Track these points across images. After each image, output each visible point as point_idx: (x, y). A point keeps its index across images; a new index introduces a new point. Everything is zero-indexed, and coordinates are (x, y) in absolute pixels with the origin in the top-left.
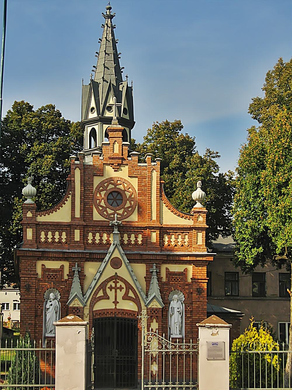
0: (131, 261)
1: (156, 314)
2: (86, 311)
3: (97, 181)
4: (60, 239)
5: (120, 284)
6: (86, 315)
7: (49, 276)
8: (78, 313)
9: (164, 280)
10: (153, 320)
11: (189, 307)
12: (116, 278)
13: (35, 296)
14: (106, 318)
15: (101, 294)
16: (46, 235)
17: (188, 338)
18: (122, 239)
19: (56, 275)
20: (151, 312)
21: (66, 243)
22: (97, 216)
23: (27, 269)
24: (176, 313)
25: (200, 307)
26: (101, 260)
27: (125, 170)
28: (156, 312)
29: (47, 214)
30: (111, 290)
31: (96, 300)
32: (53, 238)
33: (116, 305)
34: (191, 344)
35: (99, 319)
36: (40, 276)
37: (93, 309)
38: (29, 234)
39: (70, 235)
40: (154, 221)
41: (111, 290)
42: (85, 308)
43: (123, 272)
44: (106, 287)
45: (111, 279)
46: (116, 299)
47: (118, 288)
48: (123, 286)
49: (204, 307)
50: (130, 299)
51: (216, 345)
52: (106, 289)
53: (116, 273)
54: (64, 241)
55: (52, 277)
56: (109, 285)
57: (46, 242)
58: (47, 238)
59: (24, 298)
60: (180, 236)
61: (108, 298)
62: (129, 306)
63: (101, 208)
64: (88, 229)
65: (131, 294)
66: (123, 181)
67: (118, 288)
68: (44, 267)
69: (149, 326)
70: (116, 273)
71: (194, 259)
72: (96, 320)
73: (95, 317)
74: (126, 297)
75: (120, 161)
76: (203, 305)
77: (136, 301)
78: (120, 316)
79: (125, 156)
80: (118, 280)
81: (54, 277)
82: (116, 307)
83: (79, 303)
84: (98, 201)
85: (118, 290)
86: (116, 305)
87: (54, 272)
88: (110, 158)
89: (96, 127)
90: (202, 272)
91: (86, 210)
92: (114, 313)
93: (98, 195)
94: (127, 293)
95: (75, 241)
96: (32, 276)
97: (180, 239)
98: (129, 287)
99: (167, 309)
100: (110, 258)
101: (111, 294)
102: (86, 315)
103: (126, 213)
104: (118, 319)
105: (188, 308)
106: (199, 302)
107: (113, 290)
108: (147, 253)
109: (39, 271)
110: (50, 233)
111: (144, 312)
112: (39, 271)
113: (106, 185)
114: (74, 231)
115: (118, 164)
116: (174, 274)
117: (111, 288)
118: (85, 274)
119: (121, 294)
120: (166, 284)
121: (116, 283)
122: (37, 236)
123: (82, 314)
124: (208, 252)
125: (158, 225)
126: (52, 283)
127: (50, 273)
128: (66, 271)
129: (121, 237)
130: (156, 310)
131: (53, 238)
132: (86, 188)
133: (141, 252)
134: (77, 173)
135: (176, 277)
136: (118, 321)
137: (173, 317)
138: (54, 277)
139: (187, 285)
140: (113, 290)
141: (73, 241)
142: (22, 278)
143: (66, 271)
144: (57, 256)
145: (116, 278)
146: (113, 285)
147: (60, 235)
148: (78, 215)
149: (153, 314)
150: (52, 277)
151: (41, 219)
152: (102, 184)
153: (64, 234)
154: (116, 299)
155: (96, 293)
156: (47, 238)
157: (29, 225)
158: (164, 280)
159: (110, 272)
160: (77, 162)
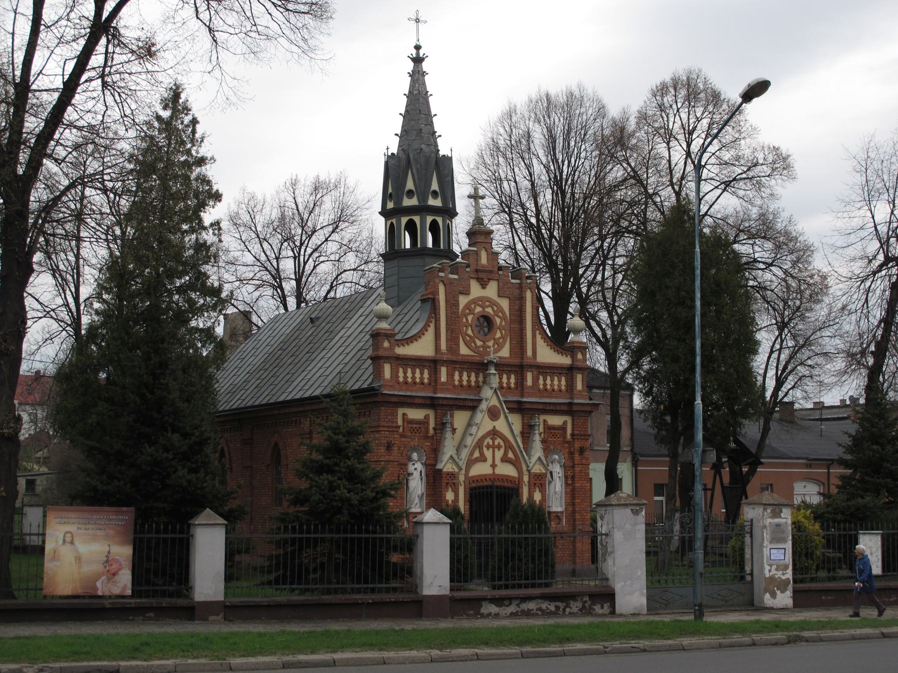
2: (462, 478)
3: (463, 301)
4: (422, 378)
5: (498, 441)
12: (494, 433)
21: (430, 384)
22: (464, 350)
31: (471, 462)
32: (413, 378)
33: (494, 470)
35: (475, 488)
39: (435, 374)
43: (501, 425)
45: (488, 434)
46: (494, 461)
48: (502, 444)
53: (494, 427)
54: (426, 381)
55: (416, 430)
56: (485, 443)
58: (405, 377)
61: (485, 460)
62: (508, 470)
70: (494, 427)
72: (471, 489)
74: (505, 459)
78: (498, 483)
82: (494, 473)
85: (496, 450)
86: (494, 470)
89: (417, 219)
91: (453, 341)
94: (506, 453)
101: (488, 454)
107: (491, 450)
110: (409, 371)
111: (526, 479)
116: (412, 422)
117: (488, 447)
119: (499, 454)
121: (493, 439)
126: (416, 439)
128: (432, 424)
131: (413, 378)
137: (553, 485)
140: (491, 450)
143: (432, 424)
145: (494, 433)
147: (422, 374)
148: (443, 346)
150: (416, 430)
152: (468, 306)
153: (426, 371)
154: (494, 461)
155: (472, 453)
156: (405, 377)
159: (487, 425)
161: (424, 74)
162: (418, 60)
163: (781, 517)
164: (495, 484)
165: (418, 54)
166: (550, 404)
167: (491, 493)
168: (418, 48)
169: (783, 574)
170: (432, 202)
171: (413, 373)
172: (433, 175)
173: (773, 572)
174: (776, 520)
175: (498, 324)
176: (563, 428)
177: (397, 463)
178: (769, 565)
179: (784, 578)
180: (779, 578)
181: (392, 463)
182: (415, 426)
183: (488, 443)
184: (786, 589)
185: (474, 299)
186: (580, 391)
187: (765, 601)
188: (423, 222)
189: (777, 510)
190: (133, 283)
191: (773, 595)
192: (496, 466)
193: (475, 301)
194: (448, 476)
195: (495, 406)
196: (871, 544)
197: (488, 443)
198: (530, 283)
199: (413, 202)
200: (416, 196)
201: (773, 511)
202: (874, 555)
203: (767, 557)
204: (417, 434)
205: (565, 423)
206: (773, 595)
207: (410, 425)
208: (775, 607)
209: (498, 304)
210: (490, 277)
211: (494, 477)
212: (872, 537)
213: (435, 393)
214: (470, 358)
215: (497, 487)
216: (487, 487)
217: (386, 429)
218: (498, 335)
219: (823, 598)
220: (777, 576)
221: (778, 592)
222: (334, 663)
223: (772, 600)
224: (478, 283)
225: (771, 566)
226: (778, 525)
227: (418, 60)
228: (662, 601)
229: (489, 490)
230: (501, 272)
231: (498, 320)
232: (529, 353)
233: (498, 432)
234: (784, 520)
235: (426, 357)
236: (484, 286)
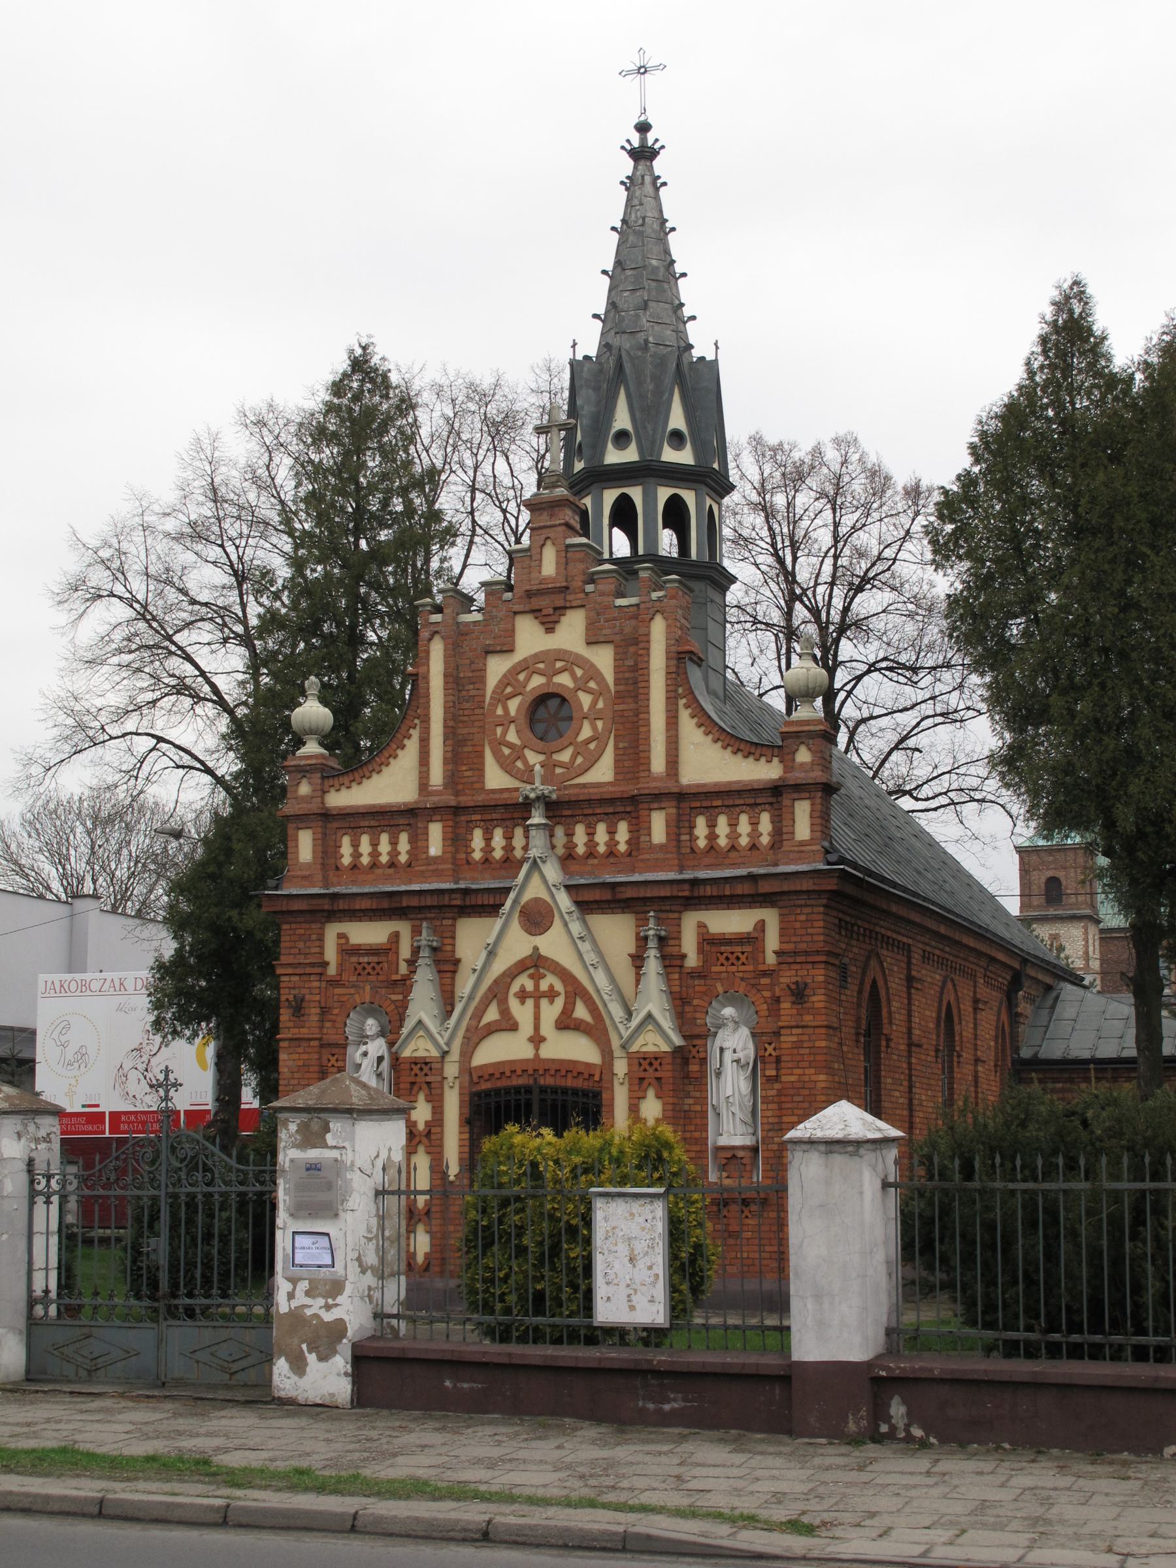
0: (585, 907)
1: (656, 1070)
2: (451, 1070)
4: (394, 853)
6: (451, 1079)
7: (360, 967)
8: (426, 1075)
9: (692, 960)
10: (645, 1091)
11: (770, 1044)
12: (536, 964)
13: (316, 1031)
14: (507, 1091)
15: (492, 1014)
16: (356, 845)
17: (770, 1147)
18: (591, 840)
19: (378, 963)
20: (640, 1064)
22: (495, 778)
23: (297, 951)
24: (729, 1069)
25: (805, 1045)
26: (493, 910)
29: (354, 784)
30: (523, 1003)
31: (477, 1035)
32: (375, 854)
33: (537, 1049)
34: (251, 1168)
35: (487, 1093)
36: (332, 970)
37: (470, 1062)
38: (305, 846)
41: (523, 1003)
42: (448, 1059)
44: (507, 992)
45: (521, 967)
46: (537, 1027)
47: (544, 995)
48: (559, 987)
49: (818, 1044)
50: (577, 1026)
51: (317, 1172)
52: (506, 998)
53: (536, 949)
55: (369, 969)
57: (712, 848)
58: (357, 855)
59: (290, 1036)
61: (513, 1027)
63: (507, 751)
64: (468, 818)
65: (581, 1012)
67: (544, 995)
68: (343, 941)
69: (634, 1109)
72: (478, 1094)
74: (566, 1023)
76: (814, 1037)
77: (596, 1031)
78: (549, 1081)
80: (542, 971)
81: (374, 968)
82: (537, 1055)
83: (430, 1046)
84: (499, 730)
85: (544, 1002)
86: (537, 1049)
87: (372, 954)
89: (636, 494)
90: (810, 931)
92: (531, 1072)
93: (500, 711)
94: (567, 1011)
95: (428, 858)
96: (308, 970)
98: (575, 990)
99: (702, 1055)
100: (515, 901)
101: (522, 1013)
102: (451, 1079)
103: (579, 760)
105: (770, 1049)
106: (798, 1027)
107: (530, 1003)
108: (637, 877)
109: (331, 954)
110: (365, 840)
111: (621, 1067)
112: (331, 954)
113: (522, 677)
114: (427, 828)
115: (555, 609)
116: (356, 950)
117: (523, 996)
118: (459, 954)
119: (551, 1012)
120: (699, 974)
121: (537, 978)
122: (327, 852)
123: (439, 1078)
124: (829, 863)
126: (368, 988)
127: (362, 960)
129: (609, 833)
130: (656, 1059)
131: (375, 854)
132: (464, 693)
133: (609, 879)
134: (437, 652)
135: (729, 948)
136: (543, 1097)
138: (374, 968)
139: (765, 974)
140: (530, 1003)
141: (424, 856)
142: (283, 978)
143: (405, 952)
144: (715, 893)
145: (536, 964)
146: (529, 986)
147: (394, 843)
148: (437, 776)
149: (645, 1070)
150: (369, 969)
151: (342, 799)
154: (537, 1027)
156: (357, 855)
157: (303, 819)
158: (692, 960)
160: (436, 618)
161: (657, 184)
162: (643, 154)
163: (326, 1146)
164: (542, 1081)
165: (643, 140)
166: (726, 880)
168: (643, 128)
169: (328, 1307)
170: (670, 455)
171: (375, 844)
172: (672, 395)
173: (301, 1299)
174: (313, 1154)
175: (586, 707)
176: (754, 939)
177: (316, 1043)
178: (289, 1279)
179: (328, 1317)
180: (316, 1316)
181: (304, 1044)
182: (366, 959)
183: (523, 987)
184: (334, 1352)
185: (525, 660)
186: (802, 843)
187: (276, 1379)
188: (649, 499)
189: (315, 1126)
191: (299, 1366)
192: (543, 1039)
193: (527, 666)
194: (416, 1069)
195: (537, 900)
196: (632, 1228)
197: (523, 987)
198: (659, 599)
199: (630, 455)
200: (688, 446)
201: (304, 1128)
202: (642, 1264)
203: (285, 1256)
205: (761, 926)
206: (299, 1366)
207: (354, 959)
208: (301, 1400)
209: (587, 661)
210: (561, 603)
211: (537, 1067)
212: (636, 1206)
213: (457, 882)
214: (506, 795)
215: (543, 1090)
216: (517, 1090)
217: (290, 971)
218: (586, 732)
219: (448, 1383)
220: (309, 1312)
221: (312, 1358)
223: (295, 1378)
224: (536, 623)
225: (294, 1281)
226: (313, 1167)
227: (643, 154)
228: (80, 1359)
230: (590, 588)
231: (585, 700)
232: (658, 764)
233: (546, 959)
234: (335, 1154)
235: (399, 805)
236: (550, 627)
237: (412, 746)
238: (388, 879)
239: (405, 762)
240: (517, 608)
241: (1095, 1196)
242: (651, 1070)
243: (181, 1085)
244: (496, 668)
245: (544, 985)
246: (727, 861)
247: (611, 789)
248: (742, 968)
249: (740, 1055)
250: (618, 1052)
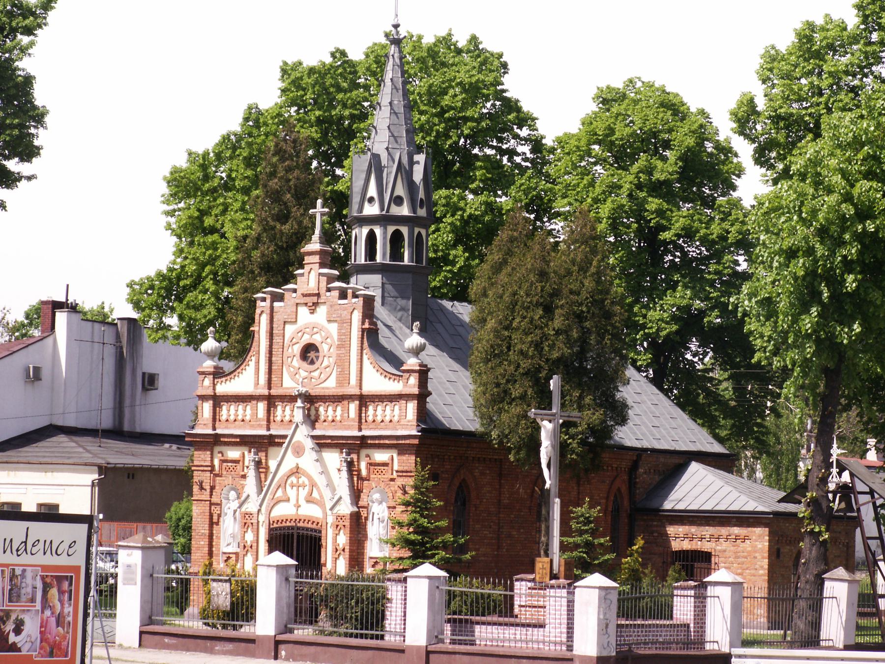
2: (262, 518)
15: (280, 493)
27: (322, 310)
28: (343, 518)
35: (276, 529)
40: (352, 388)
48: (307, 482)
55: (231, 469)
58: (375, 415)
60: (388, 407)
61: (288, 500)
66: (320, 328)
71: (395, 442)
73: (271, 527)
74: (310, 500)
75: (315, 299)
79: (323, 290)
88: (304, 295)
89: (405, 230)
97: (232, 411)
101: (291, 493)
104: (298, 528)
107: (295, 488)
115: (313, 303)
119: (303, 493)
125: (356, 391)
150: (231, 469)
156: (375, 415)
167: (293, 535)
170: (396, 210)
190: (592, 214)
204: (233, 473)
222: (745, 656)
229: (290, 531)
236: (312, 312)
237: (252, 364)
238: (240, 427)
239: (249, 370)
240: (298, 301)
241: (526, 595)
242: (341, 521)
243: (6, 210)
244: (290, 329)
245: (301, 481)
246: (379, 427)
247: (334, 390)
248: (383, 476)
249: (381, 516)
250: (329, 513)
